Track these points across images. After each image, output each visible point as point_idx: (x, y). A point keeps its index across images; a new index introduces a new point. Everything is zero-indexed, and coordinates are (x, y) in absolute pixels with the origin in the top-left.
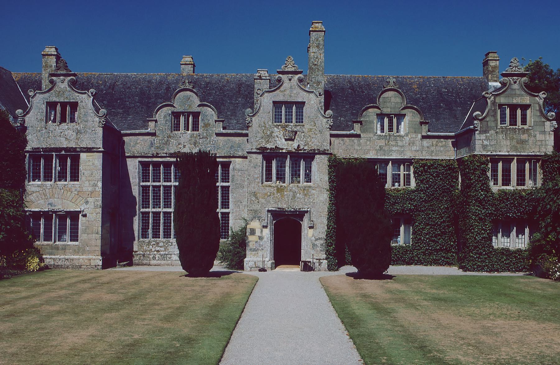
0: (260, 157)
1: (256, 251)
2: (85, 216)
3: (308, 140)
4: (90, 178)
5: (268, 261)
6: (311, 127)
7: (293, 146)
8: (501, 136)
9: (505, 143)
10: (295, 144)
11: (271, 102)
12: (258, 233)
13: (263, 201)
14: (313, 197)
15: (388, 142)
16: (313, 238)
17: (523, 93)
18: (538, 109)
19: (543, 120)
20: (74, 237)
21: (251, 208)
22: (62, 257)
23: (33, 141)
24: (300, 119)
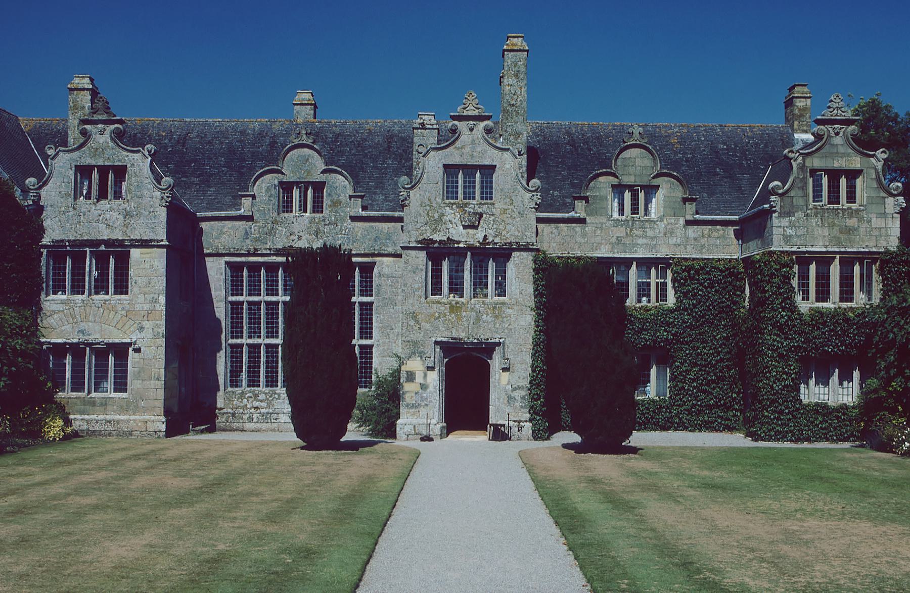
0: (423, 255)
1: (416, 407)
2: (138, 350)
3: (501, 227)
4: (147, 290)
5: (436, 424)
7: (475, 237)
9: (820, 232)
10: (479, 235)
11: (441, 166)
12: (419, 379)
13: (428, 326)
14: (509, 319)
15: (631, 230)
16: (509, 387)
17: (850, 151)
18: (874, 176)
19: (883, 194)
20: (121, 385)
21: (409, 339)
22: (101, 417)
23: (54, 230)
24: (487, 194)
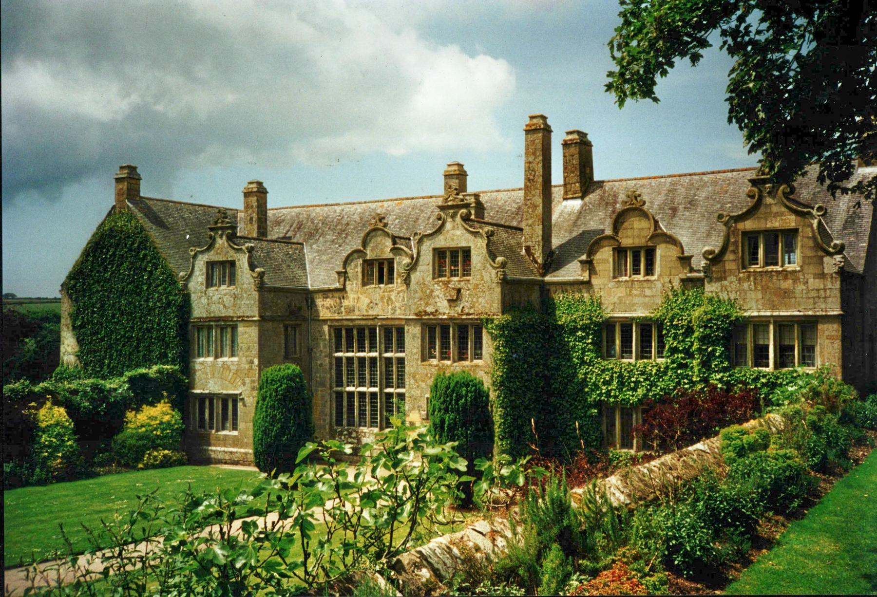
3: (474, 300)
4: (248, 353)
6: (478, 282)
8: (746, 285)
9: (753, 296)
11: (431, 249)
15: (630, 291)
17: (783, 209)
18: (810, 235)
19: (821, 253)
22: (223, 449)
23: (199, 310)
